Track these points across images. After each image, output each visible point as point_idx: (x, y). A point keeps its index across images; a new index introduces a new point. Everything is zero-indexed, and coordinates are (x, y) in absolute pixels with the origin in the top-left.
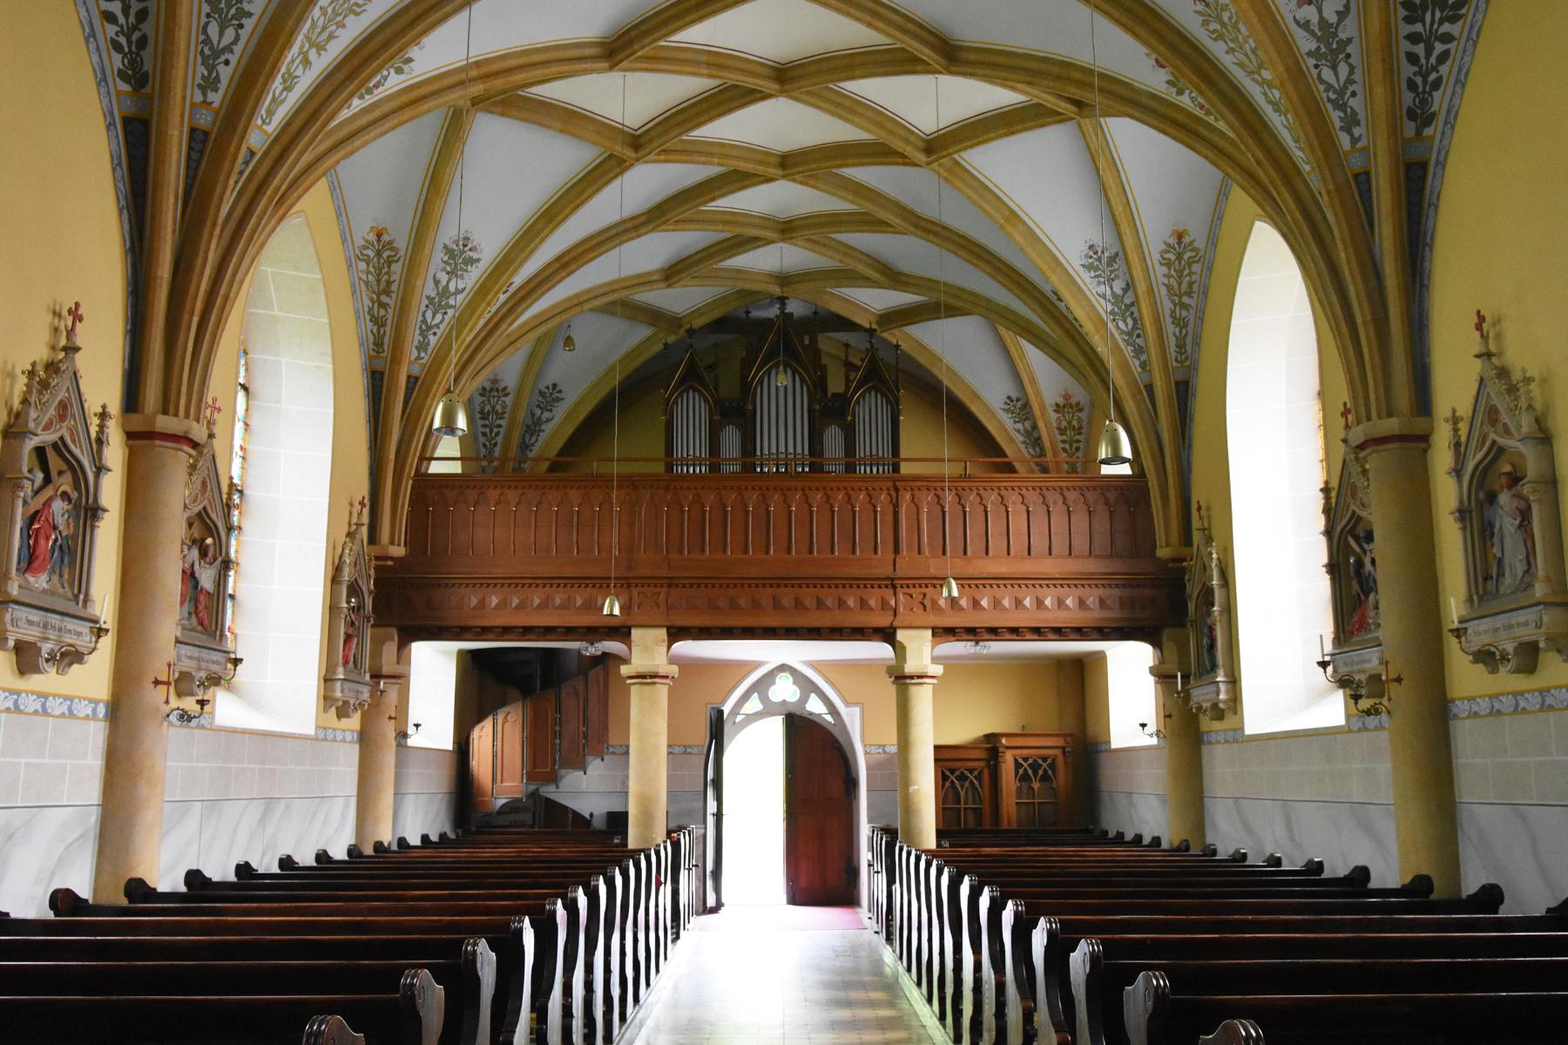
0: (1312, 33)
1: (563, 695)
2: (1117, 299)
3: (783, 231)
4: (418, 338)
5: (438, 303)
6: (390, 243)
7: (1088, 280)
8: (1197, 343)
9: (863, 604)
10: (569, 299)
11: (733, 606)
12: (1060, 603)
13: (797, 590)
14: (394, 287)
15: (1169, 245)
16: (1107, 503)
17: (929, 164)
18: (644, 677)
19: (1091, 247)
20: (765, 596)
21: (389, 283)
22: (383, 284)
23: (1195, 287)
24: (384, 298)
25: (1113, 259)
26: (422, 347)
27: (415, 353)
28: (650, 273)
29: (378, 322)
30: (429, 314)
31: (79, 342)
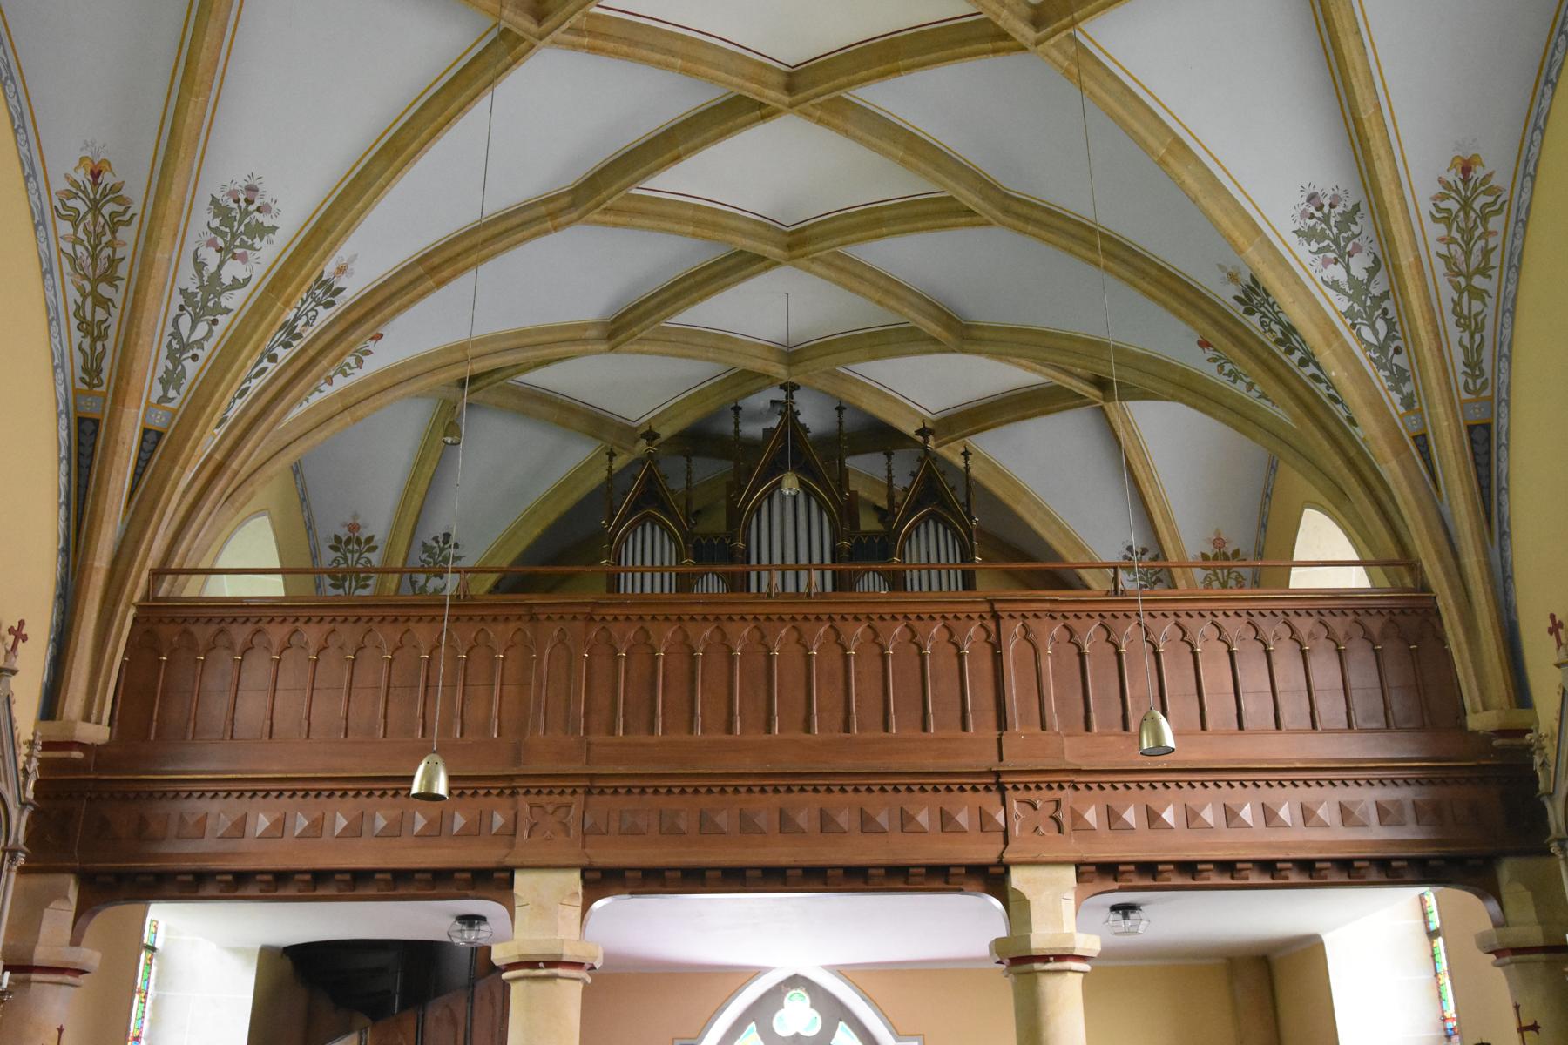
0: (1343, 292)
1: (430, 1023)
2: (1358, 289)
3: (790, 247)
4: (164, 363)
5: (203, 302)
6: (116, 188)
7: (1306, 258)
8: (1505, 355)
9: (946, 821)
10: (450, 350)
11: (706, 826)
12: (1307, 814)
13: (822, 797)
14: (122, 270)
15: (1447, 185)
16: (1367, 636)
17: (1038, 43)
18: (533, 965)
19: (1312, 198)
20: (765, 807)
21: (113, 262)
22: (103, 263)
23: (1495, 260)
24: (104, 290)
25: (1355, 216)
26: (171, 379)
27: (158, 390)
28: (584, 327)
29: (93, 331)
30: (185, 323)
31: (17, 664)
